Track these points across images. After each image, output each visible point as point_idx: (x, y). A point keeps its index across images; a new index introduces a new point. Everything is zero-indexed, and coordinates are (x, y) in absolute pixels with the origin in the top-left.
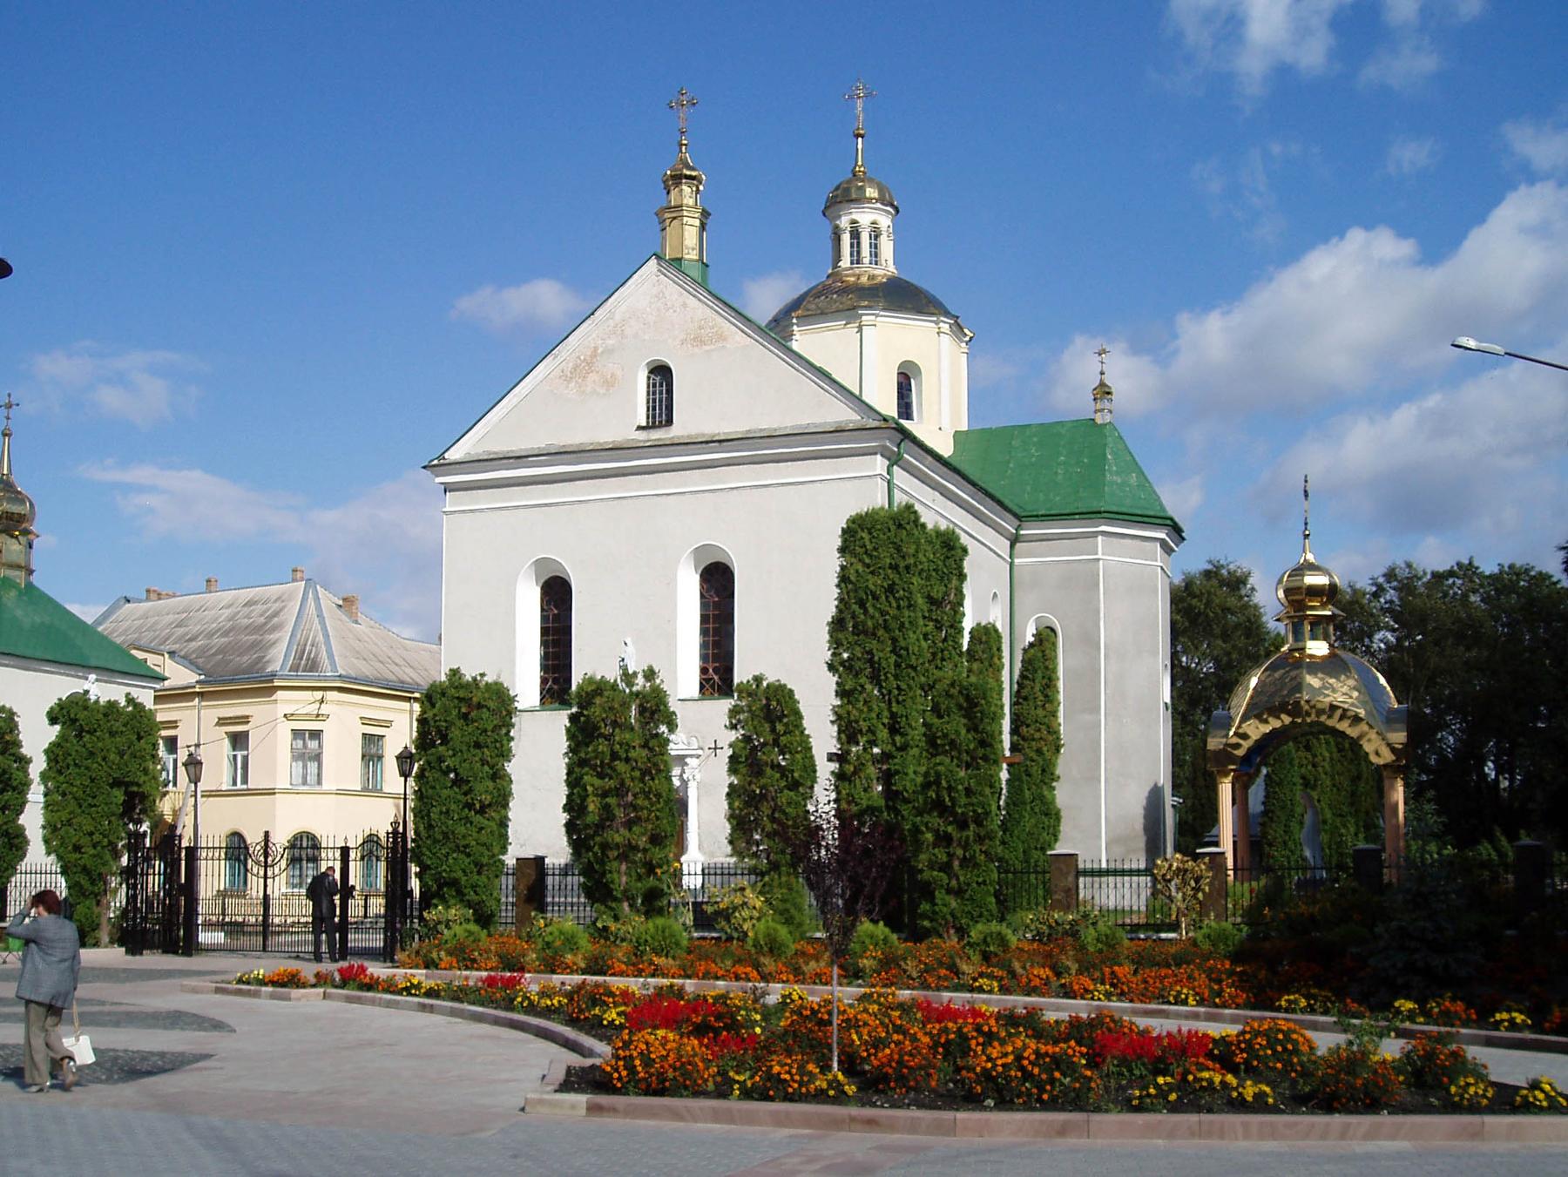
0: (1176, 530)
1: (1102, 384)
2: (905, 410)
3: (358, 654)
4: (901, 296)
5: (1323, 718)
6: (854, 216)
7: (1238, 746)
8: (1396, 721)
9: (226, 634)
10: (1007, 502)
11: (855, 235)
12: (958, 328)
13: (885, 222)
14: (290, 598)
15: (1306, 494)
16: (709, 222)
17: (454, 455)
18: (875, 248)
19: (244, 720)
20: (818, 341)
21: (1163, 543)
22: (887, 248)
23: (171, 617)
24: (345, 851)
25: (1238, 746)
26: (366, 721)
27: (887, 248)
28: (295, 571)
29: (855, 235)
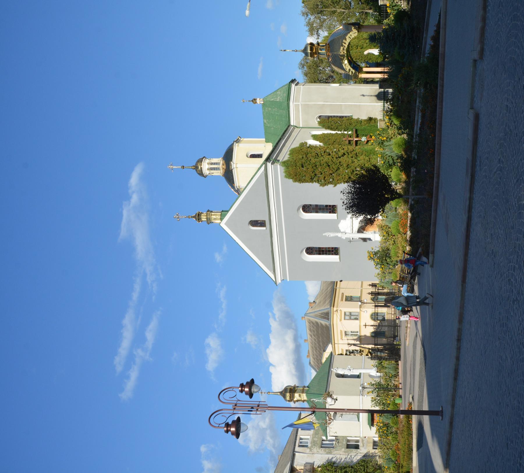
0: (293, 81)
1: (252, 101)
2: (260, 156)
3: (325, 302)
4: (228, 156)
5: (345, 49)
6: (206, 169)
7: (352, 72)
8: (409, 417)
9: (319, 337)
10: (285, 129)
11: (211, 169)
12: (238, 141)
13: (207, 161)
14: (310, 320)
15: (285, 51)
16: (210, 210)
17: (274, 280)
18: (214, 164)
19: (341, 331)
20: (240, 180)
21: (296, 85)
22: (215, 160)
23: (314, 352)
24: (376, 306)
25: (352, 72)
26: (342, 300)
27: (215, 160)
28: (198, 217)
29: (211, 169)
